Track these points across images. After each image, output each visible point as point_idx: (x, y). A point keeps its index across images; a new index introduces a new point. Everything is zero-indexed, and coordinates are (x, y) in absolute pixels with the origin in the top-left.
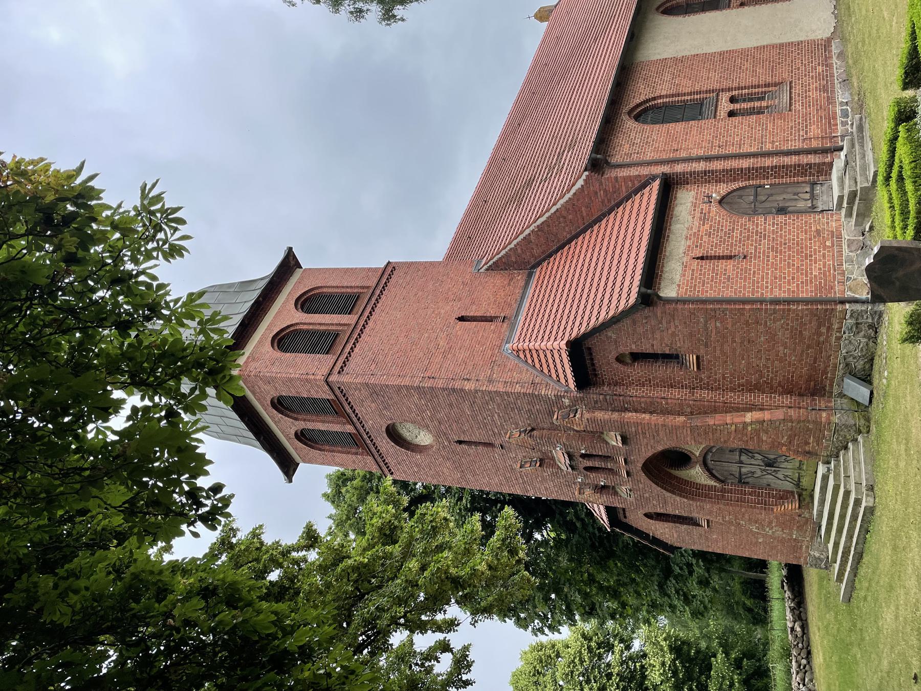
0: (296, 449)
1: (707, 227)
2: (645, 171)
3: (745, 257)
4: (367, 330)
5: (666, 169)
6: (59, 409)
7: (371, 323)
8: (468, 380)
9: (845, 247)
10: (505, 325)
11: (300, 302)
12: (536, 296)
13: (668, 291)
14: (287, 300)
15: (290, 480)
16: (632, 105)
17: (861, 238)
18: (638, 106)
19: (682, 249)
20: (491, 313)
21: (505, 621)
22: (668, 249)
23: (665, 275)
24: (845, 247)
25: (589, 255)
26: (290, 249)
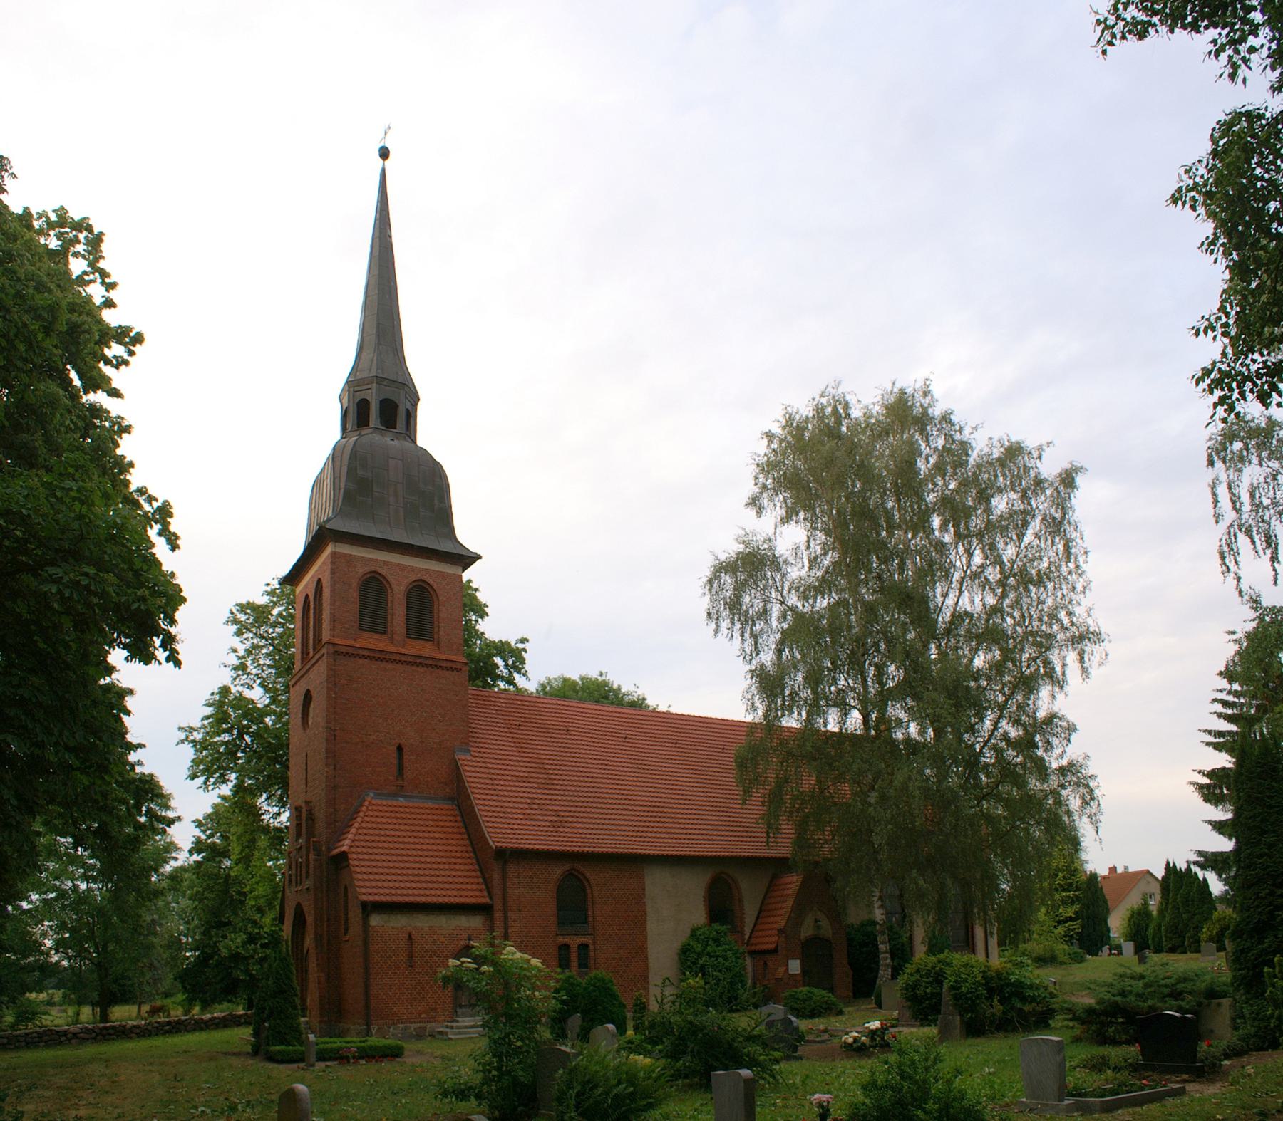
0: (412, 569)
1: (442, 939)
2: (497, 891)
3: (411, 966)
4: (384, 664)
5: (498, 906)
6: (1249, 139)
7: (390, 666)
8: (335, 769)
9: (419, 1025)
10: (394, 788)
11: (420, 583)
12: (423, 811)
13: (375, 920)
14: (420, 570)
15: (479, 557)
16: (582, 869)
17: (427, 1034)
18: (578, 871)
19: (419, 924)
20: (408, 774)
21: (619, 686)
22: (420, 916)
23: (393, 917)
24: (419, 1025)
25: (606, 796)
26: (479, 557)
